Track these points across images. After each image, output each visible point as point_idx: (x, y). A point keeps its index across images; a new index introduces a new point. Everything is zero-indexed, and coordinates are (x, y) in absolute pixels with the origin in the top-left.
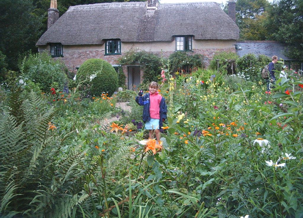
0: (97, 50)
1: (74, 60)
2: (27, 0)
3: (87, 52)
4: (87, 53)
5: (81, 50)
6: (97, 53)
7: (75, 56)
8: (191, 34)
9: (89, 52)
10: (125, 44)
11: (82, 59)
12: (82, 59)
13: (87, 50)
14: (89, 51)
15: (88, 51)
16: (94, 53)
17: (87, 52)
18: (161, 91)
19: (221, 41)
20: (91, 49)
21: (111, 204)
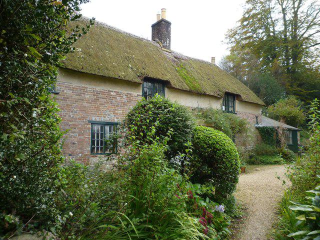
0: (130, 93)
1: (85, 104)
2: (1, 180)
3: (112, 93)
4: (111, 95)
5: (101, 88)
6: (128, 98)
7: (87, 97)
8: (165, 78)
9: (115, 94)
10: (246, 105)
11: (103, 104)
12: (103, 104)
13: (111, 90)
14: (116, 92)
15: (112, 91)
16: (125, 97)
17: (112, 93)
18: (37, 93)
19: (209, 96)
20: (118, 89)
21: (20, 128)
